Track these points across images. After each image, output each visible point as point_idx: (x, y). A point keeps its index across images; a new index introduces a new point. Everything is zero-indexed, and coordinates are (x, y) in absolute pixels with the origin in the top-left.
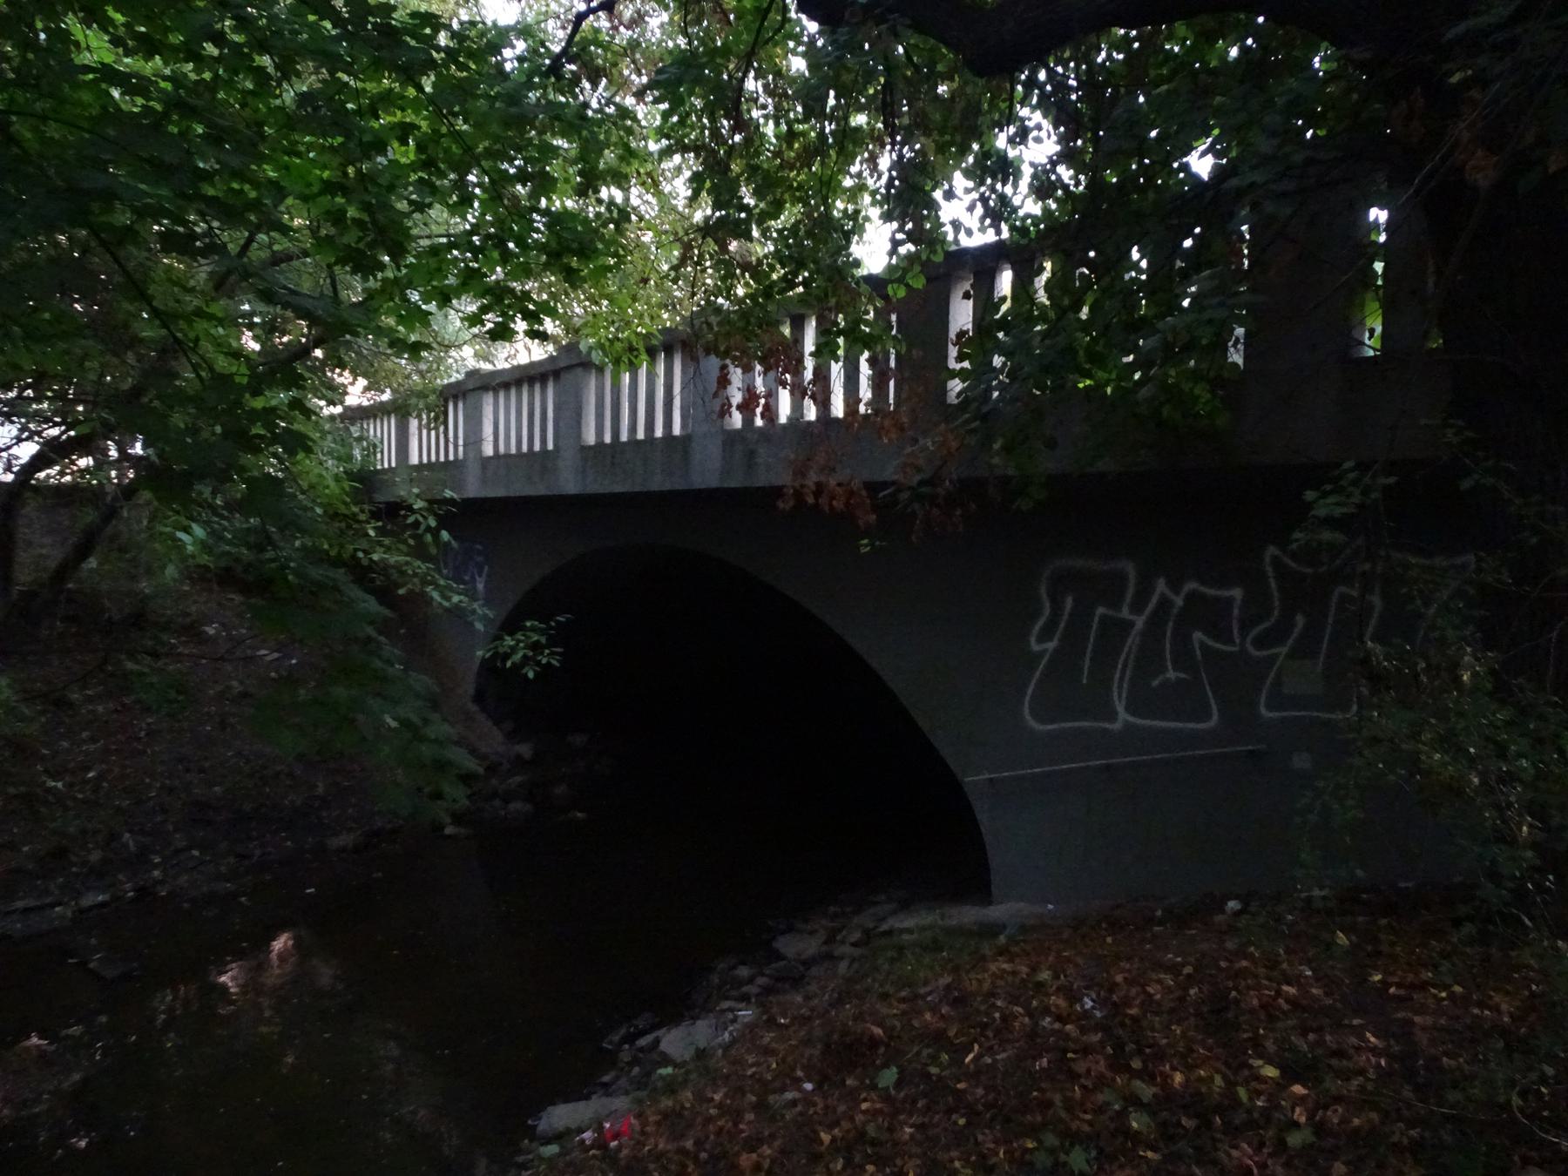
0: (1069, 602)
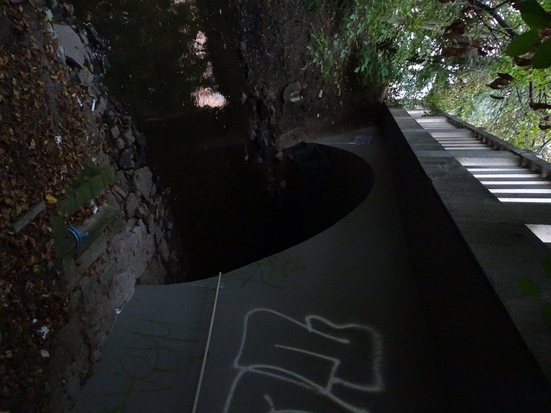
0: (345, 341)
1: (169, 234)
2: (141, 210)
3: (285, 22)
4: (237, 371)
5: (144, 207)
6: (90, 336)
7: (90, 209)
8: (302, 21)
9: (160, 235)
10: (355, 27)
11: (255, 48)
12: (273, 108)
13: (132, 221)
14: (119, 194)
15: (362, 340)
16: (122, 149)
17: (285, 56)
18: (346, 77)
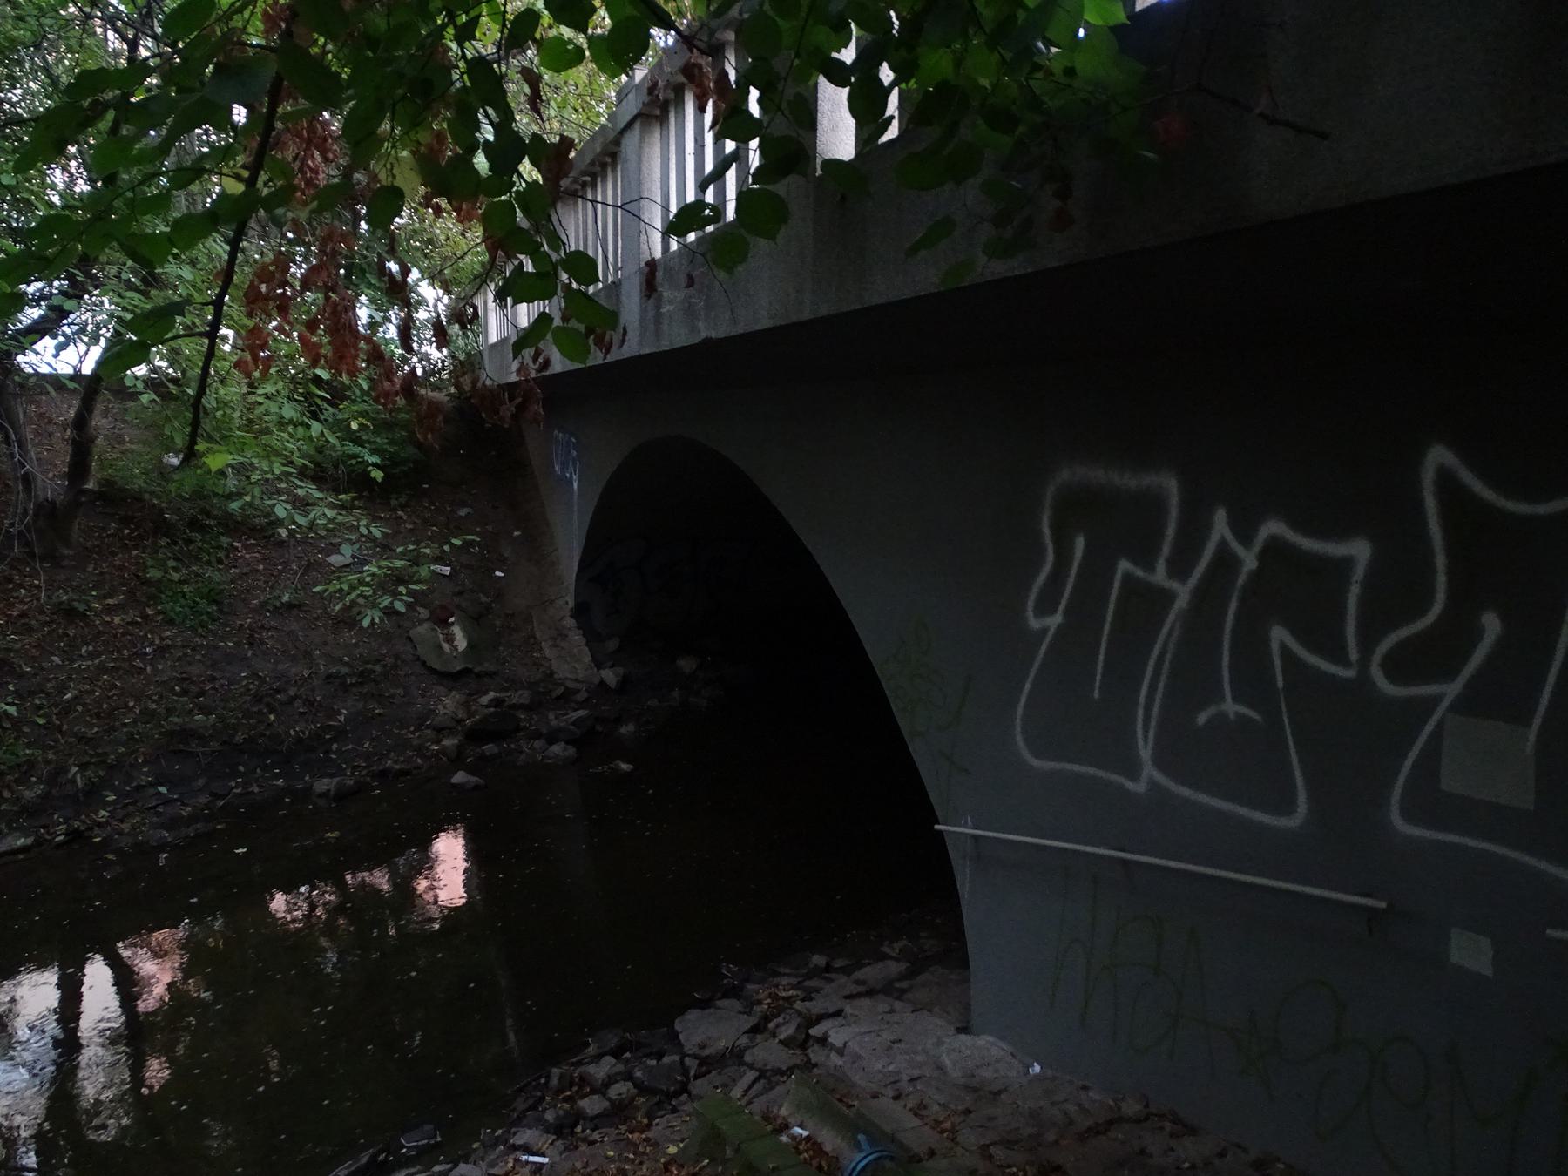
0: (1080, 543)
1: (839, 963)
2: (788, 1031)
3: (255, 675)
4: (1154, 785)
5: (778, 1026)
6: (1089, 1122)
7: (800, 1143)
8: (250, 627)
9: (844, 983)
10: (303, 505)
11: (327, 752)
12: (485, 700)
13: (816, 1054)
14: (750, 1087)
15: (1078, 508)
16: (636, 1086)
17: (345, 670)
18: (393, 502)
